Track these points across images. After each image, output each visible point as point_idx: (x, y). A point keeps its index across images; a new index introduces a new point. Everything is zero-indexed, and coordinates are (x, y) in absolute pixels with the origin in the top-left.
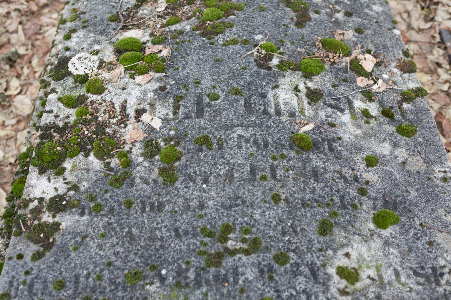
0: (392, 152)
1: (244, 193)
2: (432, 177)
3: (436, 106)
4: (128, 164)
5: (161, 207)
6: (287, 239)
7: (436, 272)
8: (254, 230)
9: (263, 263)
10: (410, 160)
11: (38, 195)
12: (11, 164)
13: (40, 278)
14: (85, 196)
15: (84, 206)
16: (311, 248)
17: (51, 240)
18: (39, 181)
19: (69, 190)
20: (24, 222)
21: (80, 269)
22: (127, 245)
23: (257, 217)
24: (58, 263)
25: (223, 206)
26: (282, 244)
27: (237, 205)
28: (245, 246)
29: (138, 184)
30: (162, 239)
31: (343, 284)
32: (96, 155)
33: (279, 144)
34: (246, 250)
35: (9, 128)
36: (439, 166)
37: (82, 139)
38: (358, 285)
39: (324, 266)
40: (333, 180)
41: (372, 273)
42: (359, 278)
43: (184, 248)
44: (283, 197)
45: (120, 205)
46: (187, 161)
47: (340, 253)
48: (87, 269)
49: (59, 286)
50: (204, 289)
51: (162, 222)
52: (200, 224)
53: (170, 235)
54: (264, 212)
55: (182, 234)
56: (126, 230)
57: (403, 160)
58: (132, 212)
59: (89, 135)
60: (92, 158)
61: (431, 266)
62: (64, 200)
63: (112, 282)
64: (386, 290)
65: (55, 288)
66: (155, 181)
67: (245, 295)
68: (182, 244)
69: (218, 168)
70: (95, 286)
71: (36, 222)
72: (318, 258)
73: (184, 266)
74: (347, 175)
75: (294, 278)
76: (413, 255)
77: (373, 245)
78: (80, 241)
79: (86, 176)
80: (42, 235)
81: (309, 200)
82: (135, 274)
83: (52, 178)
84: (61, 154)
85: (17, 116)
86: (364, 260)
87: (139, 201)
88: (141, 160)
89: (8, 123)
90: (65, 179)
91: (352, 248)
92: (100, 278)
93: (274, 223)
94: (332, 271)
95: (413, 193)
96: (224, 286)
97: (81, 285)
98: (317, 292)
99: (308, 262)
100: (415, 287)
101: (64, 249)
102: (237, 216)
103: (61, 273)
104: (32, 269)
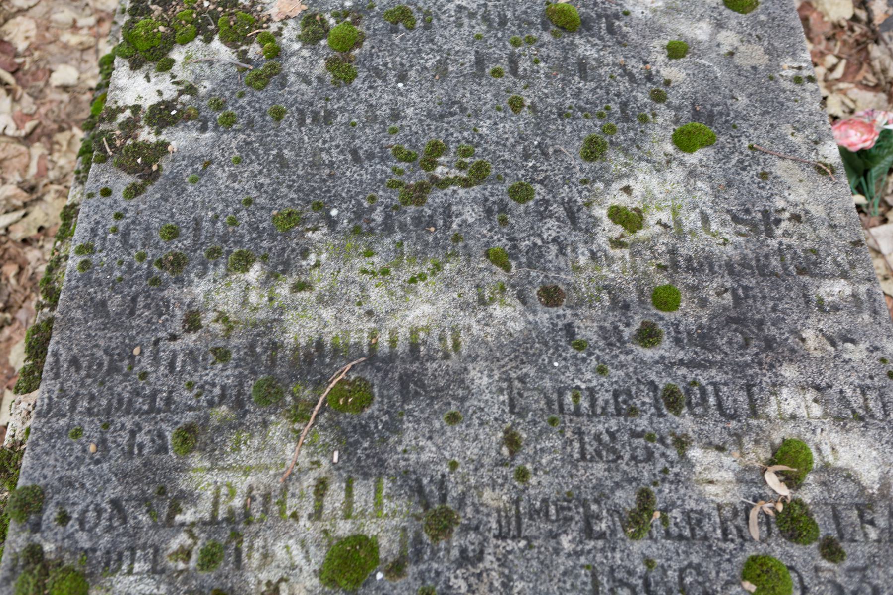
0: (713, 36)
1: (464, 96)
2: (777, 75)
4: (276, 53)
5: (330, 116)
6: (531, 164)
7: (769, 218)
8: (479, 150)
9: (491, 199)
10: (742, 48)
11: (131, 102)
12: (91, 89)
13: (140, 223)
14: (206, 102)
15: (205, 117)
16: (569, 179)
17: (155, 168)
19: (181, 93)
20: (110, 141)
21: (202, 209)
22: (275, 173)
23: (484, 131)
24: (166, 201)
25: (429, 115)
26: (523, 172)
27: (452, 114)
28: (464, 174)
29: (292, 84)
30: (331, 165)
31: (618, 230)
32: (224, 40)
33: (525, 21)
34: (465, 180)
35: (85, 31)
36: (790, 59)
37: (199, 14)
38: (641, 234)
39: (589, 205)
40: (611, 77)
41: (665, 216)
42: (644, 224)
43: (366, 177)
44: (528, 102)
45: (263, 115)
46: (373, 47)
47: (616, 186)
48: (214, 209)
49: (170, 233)
50: (398, 237)
51: (332, 139)
52: (392, 142)
53: (345, 159)
54: (495, 124)
55: (363, 157)
56: (275, 152)
57: (730, 49)
58: (283, 125)
59: (212, 7)
60: (216, 43)
61: (762, 209)
62: (174, 108)
63: (253, 227)
64: (685, 241)
65: (163, 236)
66: (320, 79)
67: (461, 244)
68: (363, 172)
69: (422, 58)
70: (226, 234)
71: (130, 142)
72: (580, 193)
73: (366, 204)
74: (634, 71)
75: (540, 220)
76: (733, 192)
77: (670, 177)
78: (201, 168)
79: (208, 72)
80: (139, 160)
81: (570, 108)
82: (289, 214)
83: (152, 75)
84: (164, 37)
85: (97, 11)
86: (654, 198)
87: (294, 108)
88: (296, 46)
89: (82, 22)
90: (173, 77)
91: (635, 179)
92: (233, 222)
93: (512, 140)
94: (601, 212)
95: (743, 100)
96: (429, 232)
98: (576, 242)
99: (563, 199)
100: (733, 238)
101: (175, 181)
102: (452, 130)
103: (172, 216)
104: (126, 210)
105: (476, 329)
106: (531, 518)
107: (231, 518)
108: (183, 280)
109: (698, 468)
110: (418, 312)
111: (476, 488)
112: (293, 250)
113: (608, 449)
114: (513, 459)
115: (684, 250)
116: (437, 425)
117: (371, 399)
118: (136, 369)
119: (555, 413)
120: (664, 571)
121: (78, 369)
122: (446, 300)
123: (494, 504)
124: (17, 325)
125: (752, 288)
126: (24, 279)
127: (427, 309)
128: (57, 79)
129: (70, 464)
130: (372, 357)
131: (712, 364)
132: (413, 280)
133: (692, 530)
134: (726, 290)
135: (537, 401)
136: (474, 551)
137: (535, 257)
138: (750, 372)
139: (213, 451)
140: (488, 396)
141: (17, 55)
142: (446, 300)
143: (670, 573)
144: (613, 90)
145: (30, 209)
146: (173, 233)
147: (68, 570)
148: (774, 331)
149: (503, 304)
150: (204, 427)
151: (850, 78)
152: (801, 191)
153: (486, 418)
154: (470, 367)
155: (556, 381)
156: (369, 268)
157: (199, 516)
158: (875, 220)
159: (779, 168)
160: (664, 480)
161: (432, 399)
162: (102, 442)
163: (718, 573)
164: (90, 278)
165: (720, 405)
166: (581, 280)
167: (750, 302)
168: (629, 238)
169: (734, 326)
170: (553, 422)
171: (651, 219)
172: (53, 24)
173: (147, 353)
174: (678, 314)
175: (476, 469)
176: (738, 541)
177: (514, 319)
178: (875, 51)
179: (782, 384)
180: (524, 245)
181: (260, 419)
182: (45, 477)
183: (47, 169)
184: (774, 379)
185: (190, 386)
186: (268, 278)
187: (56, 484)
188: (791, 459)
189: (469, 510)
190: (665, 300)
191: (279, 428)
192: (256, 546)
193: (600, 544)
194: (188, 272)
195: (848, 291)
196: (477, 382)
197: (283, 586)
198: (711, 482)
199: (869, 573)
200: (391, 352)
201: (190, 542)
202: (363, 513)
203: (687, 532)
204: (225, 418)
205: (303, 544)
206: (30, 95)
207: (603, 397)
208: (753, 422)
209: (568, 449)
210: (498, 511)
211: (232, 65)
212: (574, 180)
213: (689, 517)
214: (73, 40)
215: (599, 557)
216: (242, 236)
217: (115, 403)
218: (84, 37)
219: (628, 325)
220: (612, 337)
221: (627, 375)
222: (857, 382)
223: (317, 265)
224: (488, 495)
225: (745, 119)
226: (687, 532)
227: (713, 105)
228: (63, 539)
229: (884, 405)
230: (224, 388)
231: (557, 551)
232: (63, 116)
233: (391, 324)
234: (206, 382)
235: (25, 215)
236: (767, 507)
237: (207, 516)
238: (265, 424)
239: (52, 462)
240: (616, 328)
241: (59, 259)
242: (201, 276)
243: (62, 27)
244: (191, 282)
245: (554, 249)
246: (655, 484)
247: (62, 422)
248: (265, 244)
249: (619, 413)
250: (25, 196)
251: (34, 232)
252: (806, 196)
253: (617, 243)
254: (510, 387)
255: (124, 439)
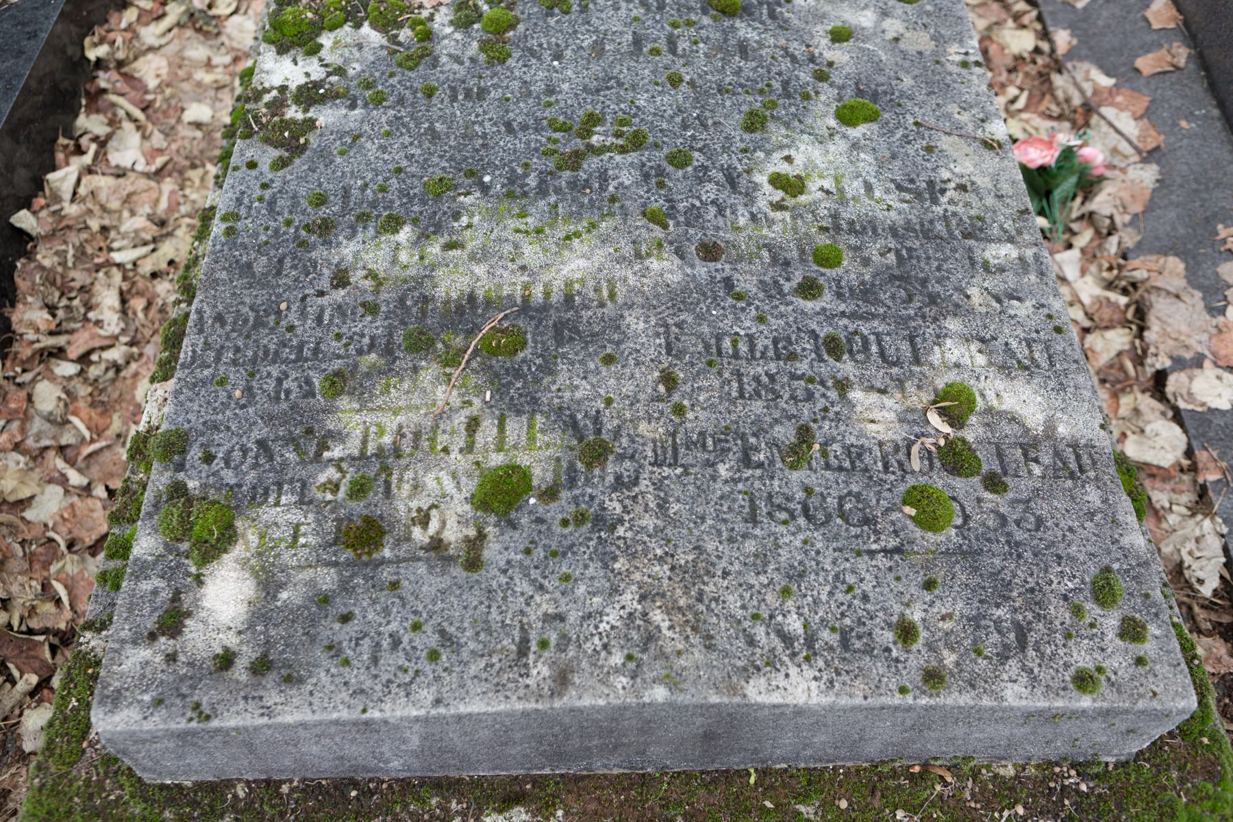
0: (877, 23)
1: (621, 72)
2: (943, 59)
3: (982, 24)
4: (427, 36)
5: (482, 93)
10: (908, 35)
14: (355, 82)
15: (354, 96)
17: (302, 141)
18: (278, 65)
19: (329, 74)
20: (256, 118)
22: (427, 145)
27: (608, 88)
28: (620, 142)
29: (444, 65)
31: (778, 195)
32: (374, 26)
34: (622, 146)
35: (220, 70)
38: (803, 199)
39: (749, 172)
41: (828, 184)
43: (520, 146)
44: (687, 78)
45: (415, 92)
47: (777, 156)
50: (553, 199)
51: (485, 113)
54: (653, 97)
56: (426, 125)
57: (895, 35)
58: (435, 100)
60: (366, 29)
63: (403, 193)
66: (472, 60)
67: (617, 205)
68: (517, 142)
71: (276, 119)
72: (740, 160)
74: (796, 53)
77: (832, 148)
79: (357, 55)
80: (286, 134)
81: (730, 84)
82: (441, 180)
83: (299, 59)
84: (312, 23)
85: (233, 49)
88: (448, 30)
89: (217, 60)
90: (321, 60)
92: (383, 189)
94: (761, 179)
95: (908, 82)
97: (353, 199)
101: (324, 154)
102: (608, 102)
103: (320, 185)
104: (272, 181)
105: (632, 280)
106: (688, 448)
107: (380, 453)
108: (331, 243)
109: (859, 408)
110: (573, 266)
111: (631, 421)
112: (445, 213)
113: (767, 389)
114: (670, 396)
115: (847, 214)
116: (592, 366)
117: (525, 343)
118: (283, 323)
119: (713, 355)
120: (824, 498)
121: (223, 324)
122: (600, 255)
123: (651, 435)
124: (144, 359)
125: (916, 250)
126: (153, 312)
127: (582, 263)
128: (188, 116)
129: (214, 409)
130: (526, 307)
131: (874, 316)
132: (568, 238)
133: (852, 463)
134: (890, 250)
135: (695, 345)
136: (629, 476)
137: (694, 216)
138: (913, 324)
139: (362, 395)
140: (644, 340)
141: (146, 92)
142: (600, 255)
143: (829, 500)
144: (774, 70)
145: (160, 244)
146: (320, 200)
147: (214, 503)
148: (938, 288)
149: (659, 258)
150: (353, 373)
151: (1032, 109)
152: (967, 164)
153: (642, 359)
154: (626, 314)
155: (715, 327)
156: (523, 227)
157: (347, 452)
158: (1059, 245)
159: (945, 142)
160: (824, 418)
161: (587, 343)
162: (248, 390)
163: (878, 501)
164: (235, 243)
165: (882, 353)
166: (741, 238)
167: (914, 262)
168: (790, 202)
169: (898, 283)
170: (710, 364)
171: (813, 186)
172: (186, 62)
173: (294, 308)
174: (840, 271)
175: (632, 404)
176: (899, 473)
177: (671, 272)
178: (1058, 80)
179: (946, 336)
180: (681, 206)
181: (410, 364)
182: (189, 422)
183: (179, 204)
184: (938, 331)
185: (338, 337)
186: (419, 238)
187: (201, 427)
188: (955, 405)
189: (625, 441)
190: (827, 259)
191: (429, 372)
192: (406, 478)
193: (758, 472)
194: (336, 235)
195: (1015, 254)
196: (633, 327)
197: (434, 512)
198: (873, 421)
199: (1032, 504)
200: (545, 303)
201: (338, 475)
202: (515, 447)
203: (847, 464)
204: (375, 364)
205: (454, 475)
206: (161, 132)
207: (760, 344)
208: (916, 369)
209: (727, 388)
210: (654, 441)
211: (382, 47)
212: (733, 149)
213: (849, 452)
214: (207, 78)
215: (757, 484)
216: (392, 202)
217: (261, 354)
218: (219, 75)
219: (788, 280)
220: (772, 290)
221: (787, 323)
222: (1022, 335)
223: (469, 226)
224: (643, 427)
225: (910, 98)
226: (847, 464)
227: (877, 85)
228: (208, 476)
229: (1050, 357)
230: (372, 338)
231: (714, 478)
232: (196, 152)
233: (546, 277)
234: (355, 333)
235: (154, 250)
236: (928, 442)
237: (356, 453)
238: (416, 370)
239: (196, 408)
240: (776, 282)
241: (197, 258)
242: (349, 238)
243: (195, 65)
244: (339, 244)
245: (712, 210)
246: (815, 421)
247: (206, 372)
248: (416, 208)
249: (778, 357)
250: (154, 230)
251: (164, 266)
252: (972, 169)
253: (778, 206)
254: (667, 333)
255: (271, 385)
